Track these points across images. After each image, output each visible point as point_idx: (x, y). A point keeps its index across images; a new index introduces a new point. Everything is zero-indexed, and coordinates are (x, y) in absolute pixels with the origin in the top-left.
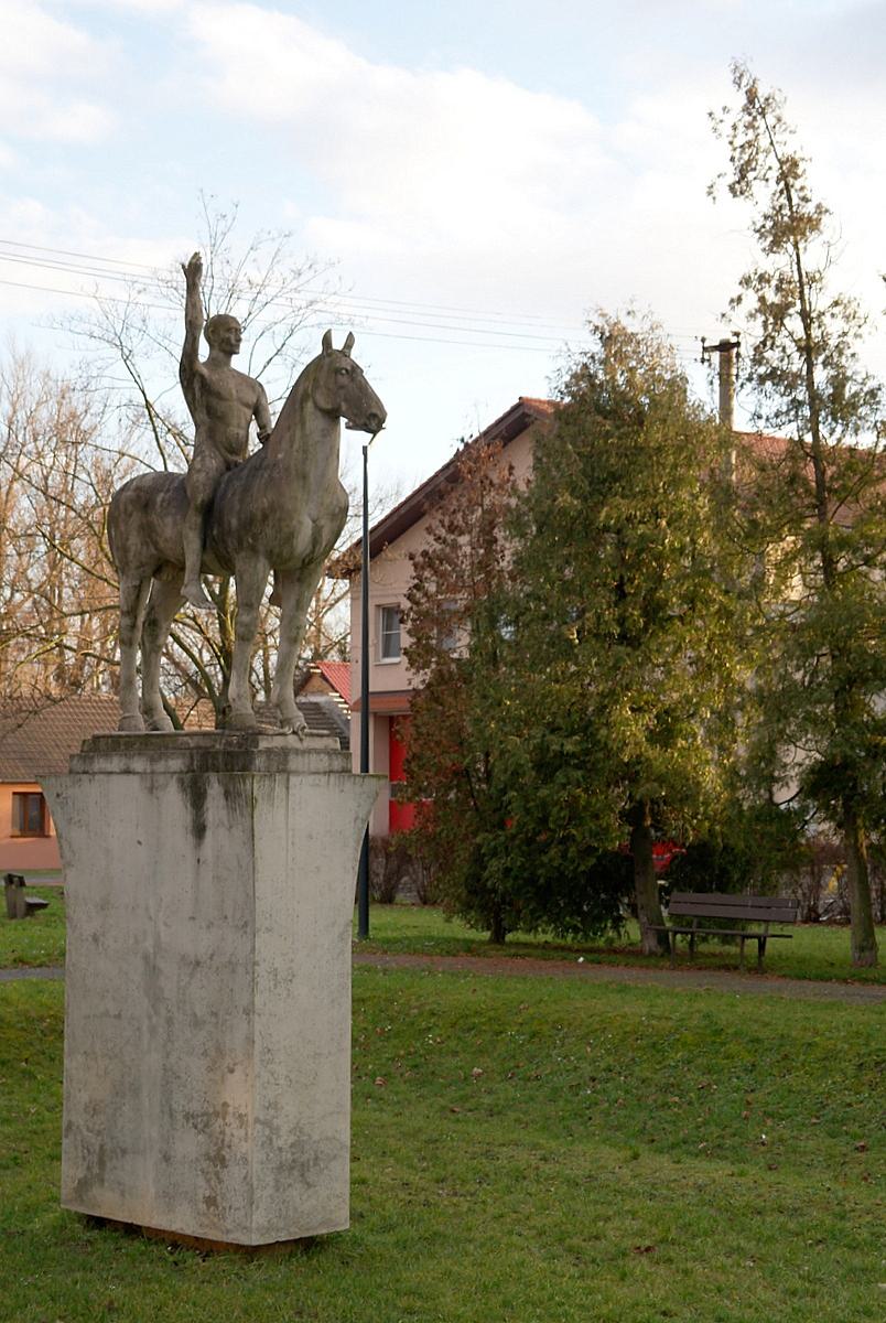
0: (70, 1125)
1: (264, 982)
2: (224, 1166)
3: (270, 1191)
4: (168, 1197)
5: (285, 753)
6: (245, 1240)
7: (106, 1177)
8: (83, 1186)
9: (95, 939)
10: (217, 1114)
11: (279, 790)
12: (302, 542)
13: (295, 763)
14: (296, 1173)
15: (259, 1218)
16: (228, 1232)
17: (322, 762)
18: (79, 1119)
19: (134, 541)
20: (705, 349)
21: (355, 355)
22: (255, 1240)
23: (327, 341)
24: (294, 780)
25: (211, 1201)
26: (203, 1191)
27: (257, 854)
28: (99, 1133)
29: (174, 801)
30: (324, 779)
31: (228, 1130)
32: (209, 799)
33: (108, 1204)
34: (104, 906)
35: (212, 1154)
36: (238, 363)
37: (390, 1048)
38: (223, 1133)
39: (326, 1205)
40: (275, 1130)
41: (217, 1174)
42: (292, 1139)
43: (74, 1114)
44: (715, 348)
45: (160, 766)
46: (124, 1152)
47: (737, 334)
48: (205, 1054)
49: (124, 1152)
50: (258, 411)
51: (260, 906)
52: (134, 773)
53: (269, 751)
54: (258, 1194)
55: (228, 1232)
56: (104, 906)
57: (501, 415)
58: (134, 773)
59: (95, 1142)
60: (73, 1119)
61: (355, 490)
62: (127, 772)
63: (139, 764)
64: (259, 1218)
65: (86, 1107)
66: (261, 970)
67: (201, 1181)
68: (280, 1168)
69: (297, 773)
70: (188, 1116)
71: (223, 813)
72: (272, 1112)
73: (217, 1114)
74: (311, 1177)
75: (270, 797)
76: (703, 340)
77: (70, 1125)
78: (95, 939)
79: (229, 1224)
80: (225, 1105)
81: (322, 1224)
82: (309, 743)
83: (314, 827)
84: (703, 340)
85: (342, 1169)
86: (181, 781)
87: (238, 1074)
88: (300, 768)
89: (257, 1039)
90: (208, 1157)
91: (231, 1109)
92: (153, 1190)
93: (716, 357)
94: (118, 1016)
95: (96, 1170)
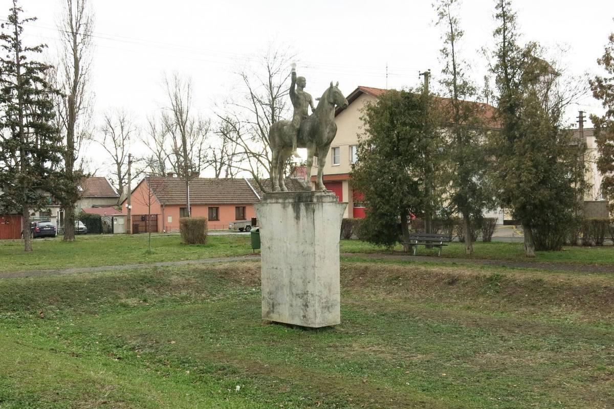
0: (264, 298)
1: (317, 259)
2: (308, 307)
3: (320, 313)
4: (292, 316)
5: (321, 197)
6: (314, 326)
7: (275, 310)
8: (268, 313)
9: (269, 248)
10: (305, 294)
11: (320, 207)
12: (325, 141)
13: (140, 219)
14: (327, 309)
15: (318, 321)
16: (310, 324)
17: (331, 199)
18: (266, 296)
19: (277, 139)
20: (420, 75)
21: (339, 87)
22: (317, 326)
23: (331, 84)
24: (324, 204)
25: (304, 317)
26: (302, 314)
27: (315, 224)
28: (272, 299)
29: (290, 209)
30: (332, 204)
31: (308, 298)
32: (301, 210)
33: (275, 317)
34: (271, 239)
35: (304, 304)
36: (305, 90)
37: (351, 277)
38: (307, 299)
39: (334, 317)
40: (321, 298)
41: (306, 309)
42: (325, 300)
43: (265, 294)
44: (422, 74)
45: (287, 201)
46: (279, 304)
47: (429, 70)
48: (301, 278)
49: (279, 304)
50: (310, 103)
51: (316, 238)
52: (279, 203)
53: (317, 197)
54: (317, 314)
55: (310, 324)
56: (271, 239)
57: (352, 92)
58: (279, 203)
59: (271, 302)
60: (265, 295)
61: (59, 64)
62: (277, 203)
63: (280, 201)
64: (318, 321)
65: (268, 293)
66: (316, 256)
67: (302, 311)
68: (323, 308)
69: (324, 202)
70: (297, 295)
71: (305, 214)
72: (320, 293)
73: (305, 294)
74: (330, 310)
75: (319, 209)
76: (419, 72)
77: (264, 298)
78: (269, 248)
79: (309, 322)
80: (307, 291)
81: (334, 322)
82: (327, 194)
83: (331, 215)
84: (419, 72)
85: (338, 308)
86: (292, 205)
87: (311, 283)
88: (326, 201)
89: (316, 273)
90: (303, 305)
91: (309, 293)
92: (288, 314)
93: (423, 77)
94: (276, 268)
95: (271, 309)
